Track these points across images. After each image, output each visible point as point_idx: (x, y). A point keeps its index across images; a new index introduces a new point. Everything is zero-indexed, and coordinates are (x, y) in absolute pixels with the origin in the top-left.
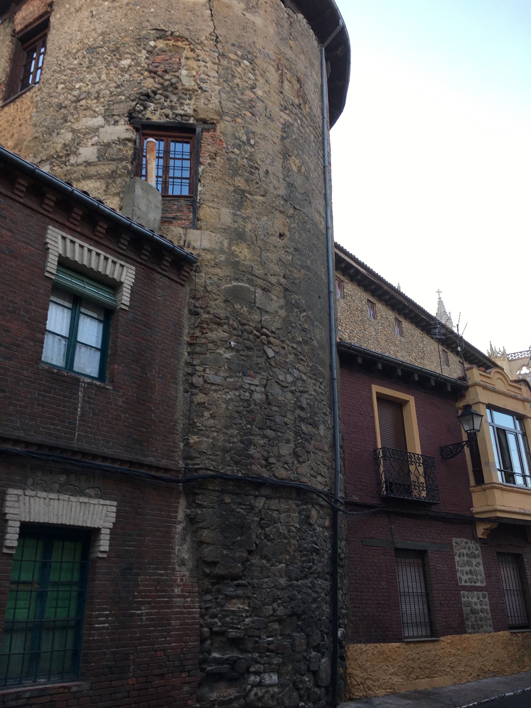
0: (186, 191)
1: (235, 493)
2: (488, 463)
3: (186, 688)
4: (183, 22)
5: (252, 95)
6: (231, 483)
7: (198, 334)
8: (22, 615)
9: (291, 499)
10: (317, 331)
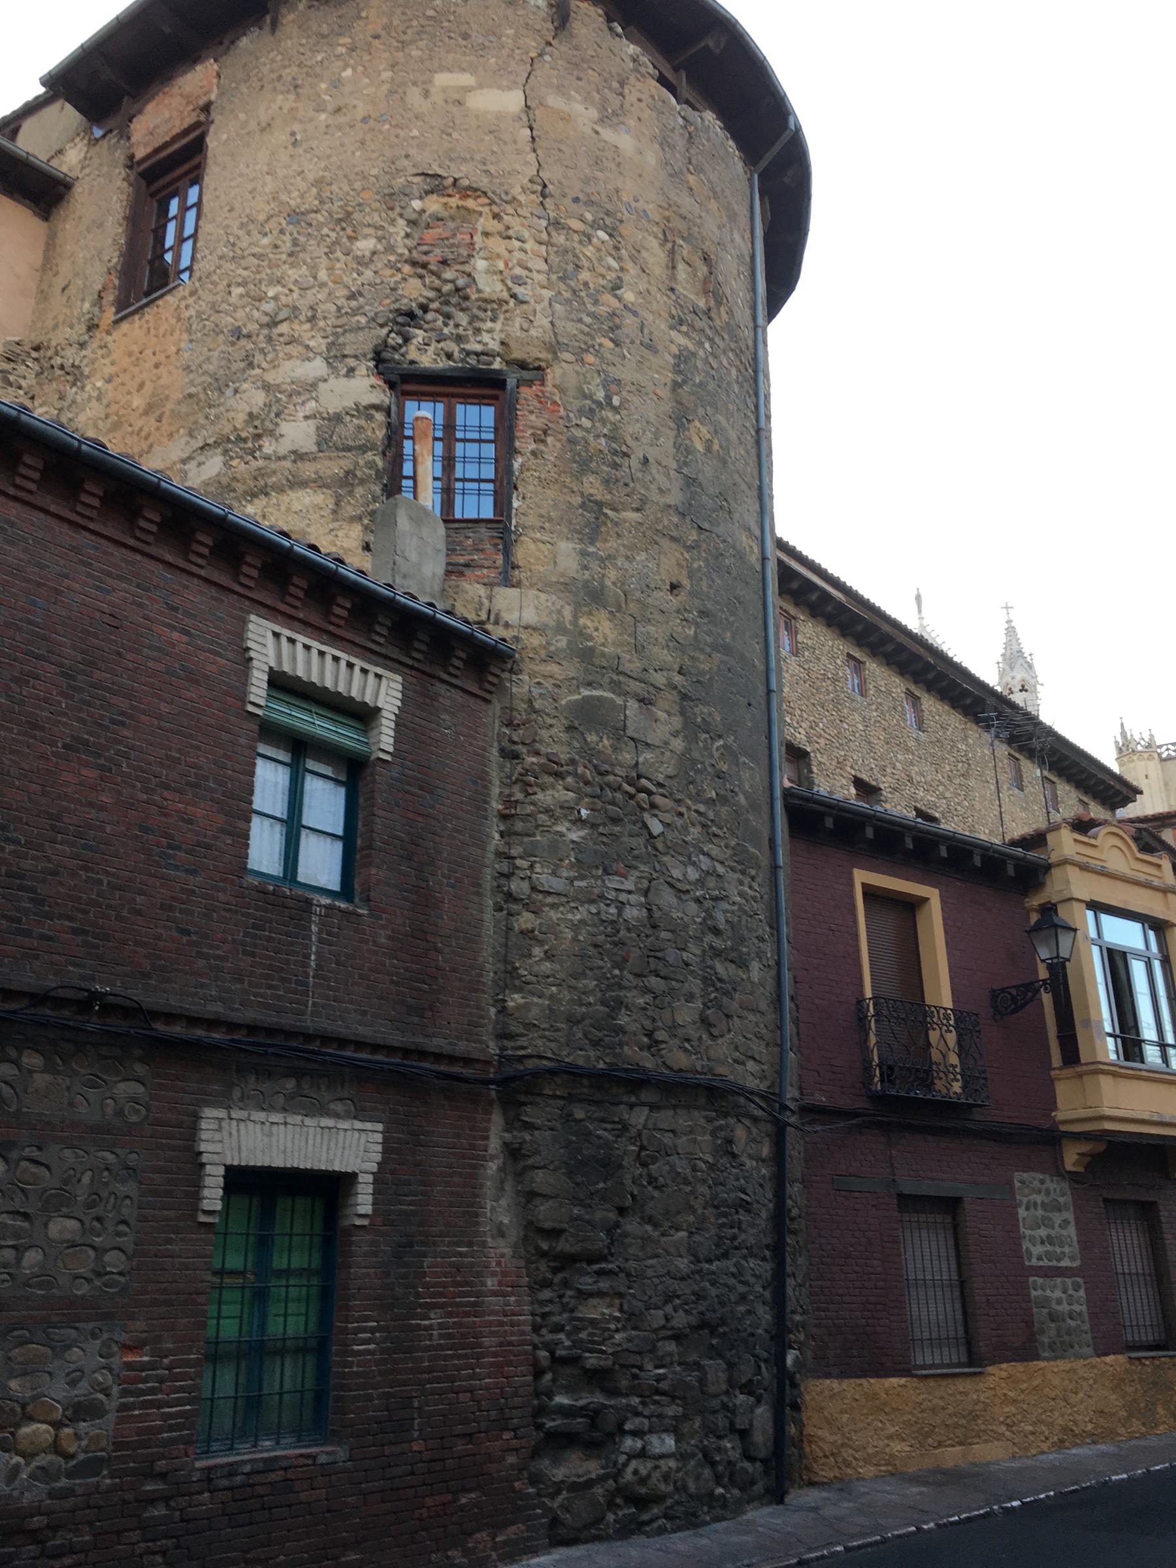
0: (488, 512)
1: (593, 1101)
2: (1087, 1022)
3: (511, 1459)
4: (478, 157)
5: (614, 303)
6: (585, 1082)
7: (519, 796)
8: (229, 1329)
9: (697, 1108)
10: (746, 775)
